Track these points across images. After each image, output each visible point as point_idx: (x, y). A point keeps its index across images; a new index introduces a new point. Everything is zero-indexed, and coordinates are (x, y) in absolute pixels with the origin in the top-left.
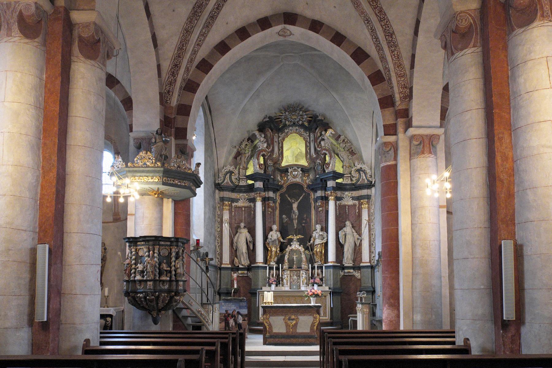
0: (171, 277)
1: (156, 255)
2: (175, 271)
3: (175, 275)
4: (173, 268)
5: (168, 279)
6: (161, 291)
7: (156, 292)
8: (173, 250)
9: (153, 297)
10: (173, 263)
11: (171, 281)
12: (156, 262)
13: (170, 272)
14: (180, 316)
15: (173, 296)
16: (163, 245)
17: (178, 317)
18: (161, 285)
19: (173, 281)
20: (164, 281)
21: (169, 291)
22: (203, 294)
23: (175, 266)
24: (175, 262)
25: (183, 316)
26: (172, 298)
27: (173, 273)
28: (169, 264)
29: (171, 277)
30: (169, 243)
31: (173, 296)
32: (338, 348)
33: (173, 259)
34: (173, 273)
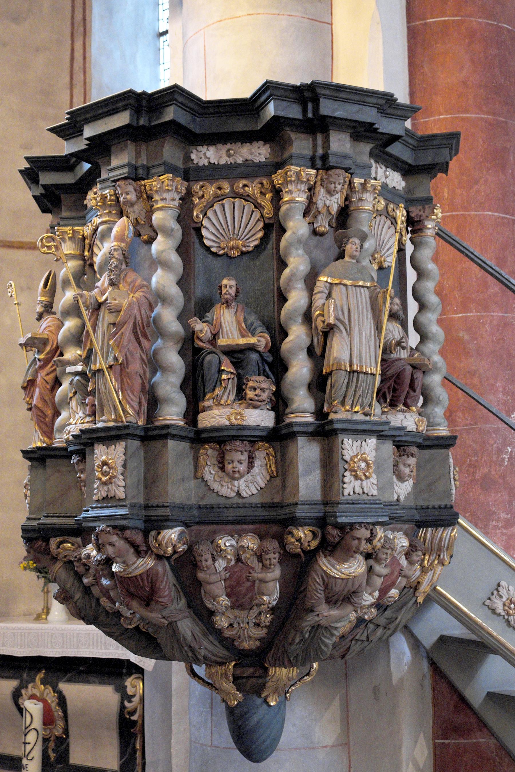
0: (280, 403)
1: (161, 246)
2: (316, 354)
3: (319, 384)
4: (297, 335)
5: (261, 418)
6: (210, 518)
7: (154, 524)
8: (296, 196)
9: (146, 563)
10: (297, 298)
11: (280, 436)
12: (161, 297)
13: (276, 366)
14: (476, 694)
15: (311, 556)
16: (213, 173)
17: (463, 703)
18: (210, 473)
19: (164, 434)
20: (221, 439)
21: (273, 518)
22: (366, 631)
23: (308, 317)
24: (311, 280)
25: (491, 696)
26: (299, 568)
27: (300, 369)
28: (268, 311)
29: (280, 403)
30: (259, 153)
31: (311, 556)
32: (167, 14)
33: (298, 263)
34: (300, 369)
